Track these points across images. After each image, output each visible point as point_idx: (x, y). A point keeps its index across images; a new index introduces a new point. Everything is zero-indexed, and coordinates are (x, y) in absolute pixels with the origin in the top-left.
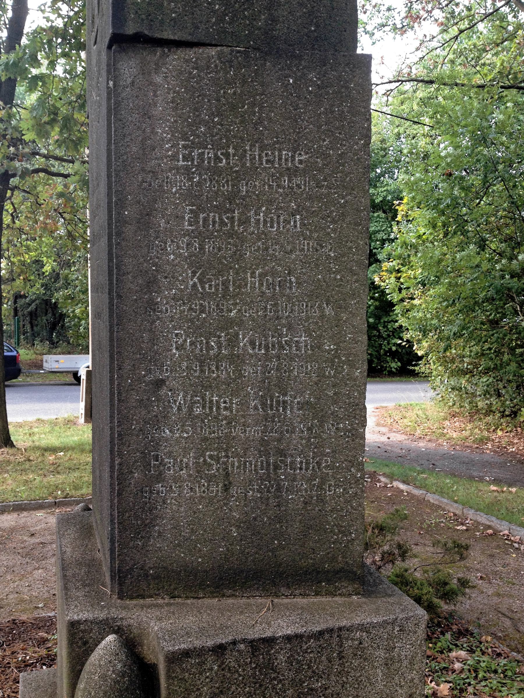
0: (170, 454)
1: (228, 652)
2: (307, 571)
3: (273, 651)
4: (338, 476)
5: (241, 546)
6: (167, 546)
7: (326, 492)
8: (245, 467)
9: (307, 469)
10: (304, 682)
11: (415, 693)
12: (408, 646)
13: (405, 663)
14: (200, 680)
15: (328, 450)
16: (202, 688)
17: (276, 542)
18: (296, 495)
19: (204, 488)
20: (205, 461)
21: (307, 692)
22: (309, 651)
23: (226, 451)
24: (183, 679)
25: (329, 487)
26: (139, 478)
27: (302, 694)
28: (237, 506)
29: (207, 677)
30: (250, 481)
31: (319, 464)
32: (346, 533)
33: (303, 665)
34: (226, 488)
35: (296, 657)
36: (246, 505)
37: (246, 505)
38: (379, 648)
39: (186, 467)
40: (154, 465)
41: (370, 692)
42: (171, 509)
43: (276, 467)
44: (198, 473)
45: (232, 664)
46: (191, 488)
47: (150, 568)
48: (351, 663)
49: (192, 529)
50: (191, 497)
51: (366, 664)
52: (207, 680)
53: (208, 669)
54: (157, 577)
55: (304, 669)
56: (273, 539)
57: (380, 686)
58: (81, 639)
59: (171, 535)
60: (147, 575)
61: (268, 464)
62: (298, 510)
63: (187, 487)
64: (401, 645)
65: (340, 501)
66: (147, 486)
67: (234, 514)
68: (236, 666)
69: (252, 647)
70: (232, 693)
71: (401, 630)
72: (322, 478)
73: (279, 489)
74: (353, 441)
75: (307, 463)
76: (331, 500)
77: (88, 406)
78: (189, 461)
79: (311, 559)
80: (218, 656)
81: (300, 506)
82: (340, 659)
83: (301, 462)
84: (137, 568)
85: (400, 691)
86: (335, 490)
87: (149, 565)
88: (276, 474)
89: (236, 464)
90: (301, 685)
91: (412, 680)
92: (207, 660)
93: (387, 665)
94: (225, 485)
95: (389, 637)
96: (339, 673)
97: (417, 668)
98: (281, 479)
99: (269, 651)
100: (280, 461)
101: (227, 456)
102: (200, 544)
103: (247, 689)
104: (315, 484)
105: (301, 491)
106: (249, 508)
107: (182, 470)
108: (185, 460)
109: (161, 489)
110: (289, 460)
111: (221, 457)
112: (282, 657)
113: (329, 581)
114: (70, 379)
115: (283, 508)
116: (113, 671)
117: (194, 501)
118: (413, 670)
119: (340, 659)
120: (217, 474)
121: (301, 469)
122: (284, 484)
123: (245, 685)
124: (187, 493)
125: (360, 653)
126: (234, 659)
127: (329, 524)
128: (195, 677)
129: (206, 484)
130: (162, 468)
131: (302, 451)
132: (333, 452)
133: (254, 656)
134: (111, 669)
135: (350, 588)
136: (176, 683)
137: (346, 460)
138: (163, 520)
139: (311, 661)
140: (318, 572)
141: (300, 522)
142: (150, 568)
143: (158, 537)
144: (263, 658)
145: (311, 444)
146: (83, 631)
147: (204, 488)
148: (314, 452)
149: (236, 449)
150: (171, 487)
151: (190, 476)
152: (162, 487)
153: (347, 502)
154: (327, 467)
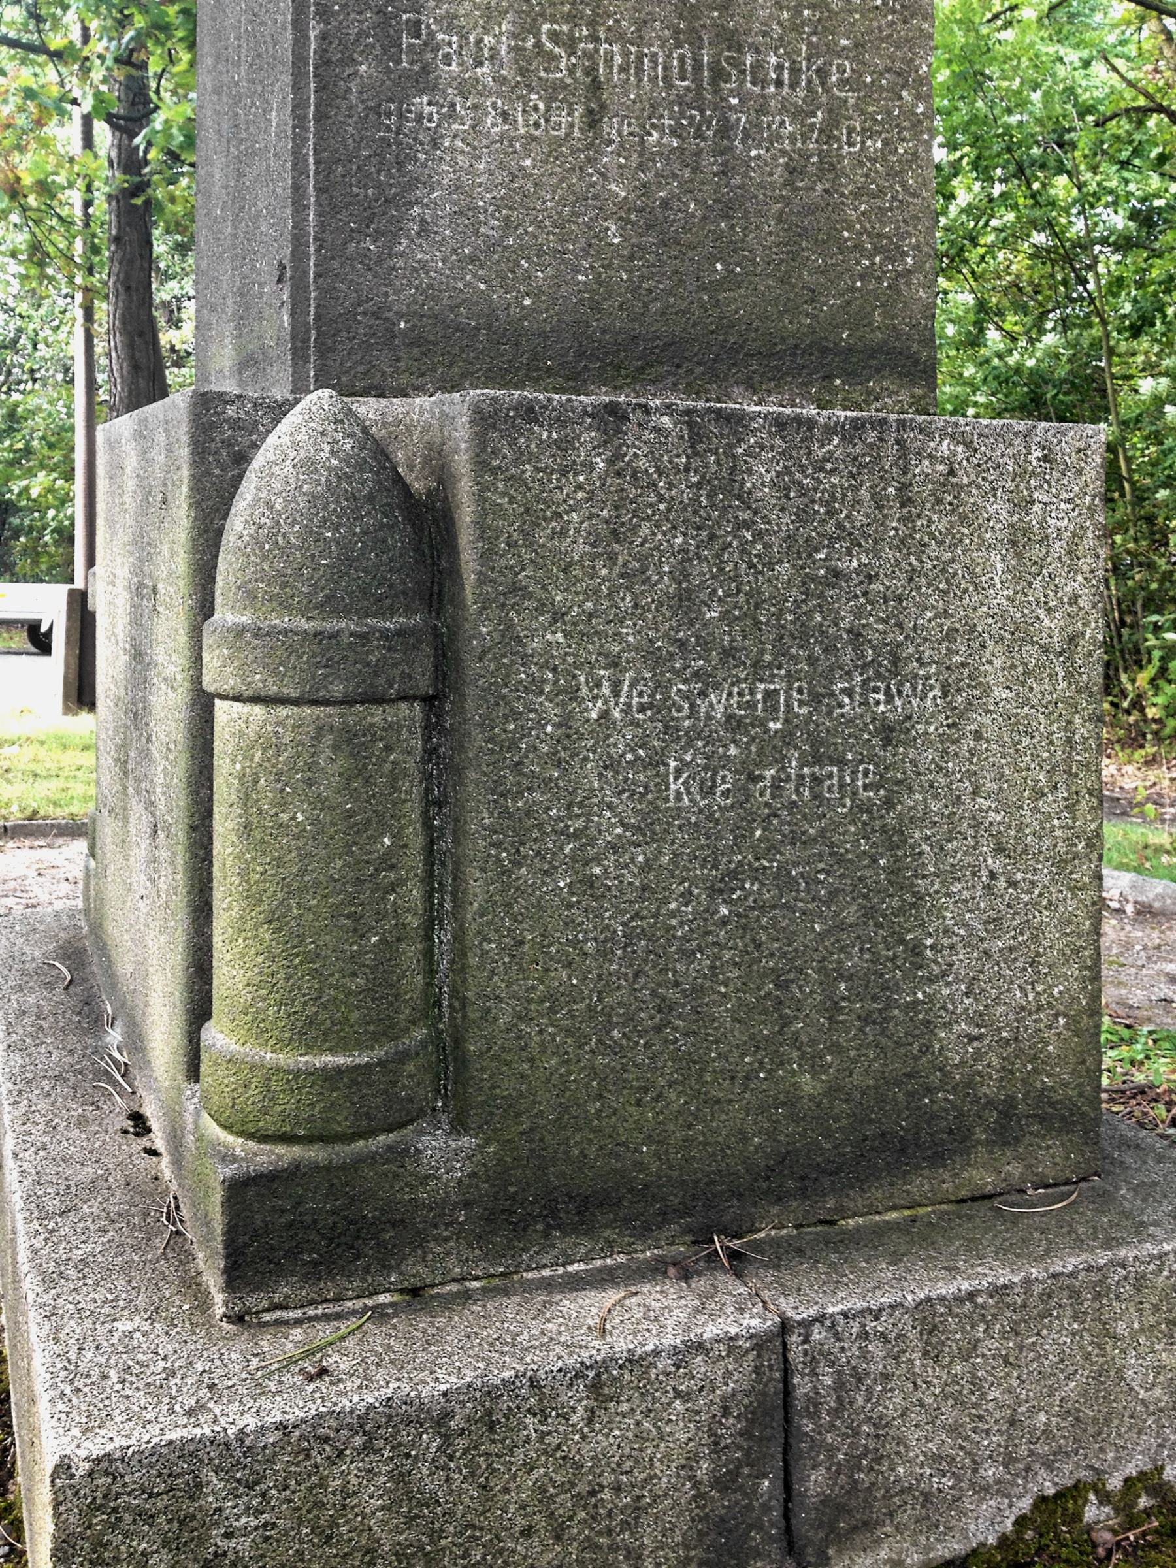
0: (449, 23)
1: (631, 428)
2: (796, 346)
3: (740, 451)
4: (871, 109)
5: (630, 272)
6: (443, 261)
7: (840, 147)
8: (639, 70)
9: (793, 85)
10: (817, 551)
11: (1083, 634)
12: (1063, 506)
13: (1059, 547)
14: (560, 488)
15: (844, 42)
16: (567, 513)
17: (719, 266)
18: (768, 150)
19: (536, 116)
20: (538, 45)
21: (825, 577)
22: (829, 466)
23: (592, 24)
24: (519, 479)
25: (849, 134)
26: (370, 77)
27: (813, 580)
28: (620, 166)
29: (580, 487)
30: (652, 106)
31: (823, 73)
32: (894, 253)
33: (813, 502)
34: (593, 121)
35: (798, 476)
36: (641, 167)
37: (641, 167)
38: (995, 496)
39: (492, 57)
40: (410, 45)
41: (975, 609)
42: (454, 163)
43: (719, 75)
44: (522, 75)
45: (642, 464)
46: (505, 115)
47: (401, 315)
48: (930, 521)
49: (507, 219)
50: (503, 136)
51: (966, 531)
52: (580, 495)
53: (583, 464)
54: (415, 340)
55: (816, 512)
56: (712, 259)
57: (999, 598)
58: (228, 444)
59: (453, 231)
60: (391, 334)
61: (698, 67)
62: (772, 185)
63: (495, 108)
64: (1046, 500)
65: (877, 172)
66: (391, 100)
67: (613, 187)
68: (652, 470)
69: (689, 424)
70: (642, 544)
71: (1045, 459)
72: (830, 111)
73: (726, 130)
74: (905, 22)
75: (795, 71)
76: (853, 168)
77: (73, 675)
78: (499, 42)
79: (807, 315)
80: (605, 433)
81: (779, 175)
82: (903, 505)
83: (779, 68)
84: (364, 313)
85: (1047, 622)
86: (863, 142)
87: (395, 308)
88: (717, 91)
89: (618, 60)
90: (810, 556)
91: (1074, 599)
92: (579, 436)
93: (1014, 543)
94: (590, 112)
95: (1019, 471)
96: (902, 542)
97: (1085, 568)
98: (731, 108)
99: (731, 446)
100: (728, 59)
101: (595, 39)
102: (528, 259)
103: (679, 541)
104: (814, 124)
105: (779, 138)
106: (651, 175)
107: (481, 64)
108: (488, 40)
109: (427, 109)
110: (749, 60)
111: (580, 40)
112: (763, 471)
113: (850, 376)
114: (21, 640)
115: (737, 180)
116: (332, 452)
117: (511, 146)
118: (1076, 572)
119: (903, 505)
120: (568, 81)
121: (779, 83)
122: (739, 119)
123: (674, 528)
124: (494, 125)
125: (949, 498)
126: (646, 450)
127: (850, 229)
128: (550, 481)
129: (541, 106)
130: (430, 55)
131: (781, 39)
132: (856, 46)
133: (696, 454)
134: (327, 448)
135: (905, 396)
136: (501, 485)
137: (889, 70)
138: (433, 190)
139: (832, 496)
140: (825, 351)
141: (779, 220)
142: (401, 315)
143: (418, 233)
144: (718, 462)
145: (803, 24)
146: (236, 424)
147: (536, 116)
148: (810, 45)
149: (617, 21)
150: (453, 105)
151: (501, 80)
152: (429, 104)
153: (891, 174)
154: (843, 82)
